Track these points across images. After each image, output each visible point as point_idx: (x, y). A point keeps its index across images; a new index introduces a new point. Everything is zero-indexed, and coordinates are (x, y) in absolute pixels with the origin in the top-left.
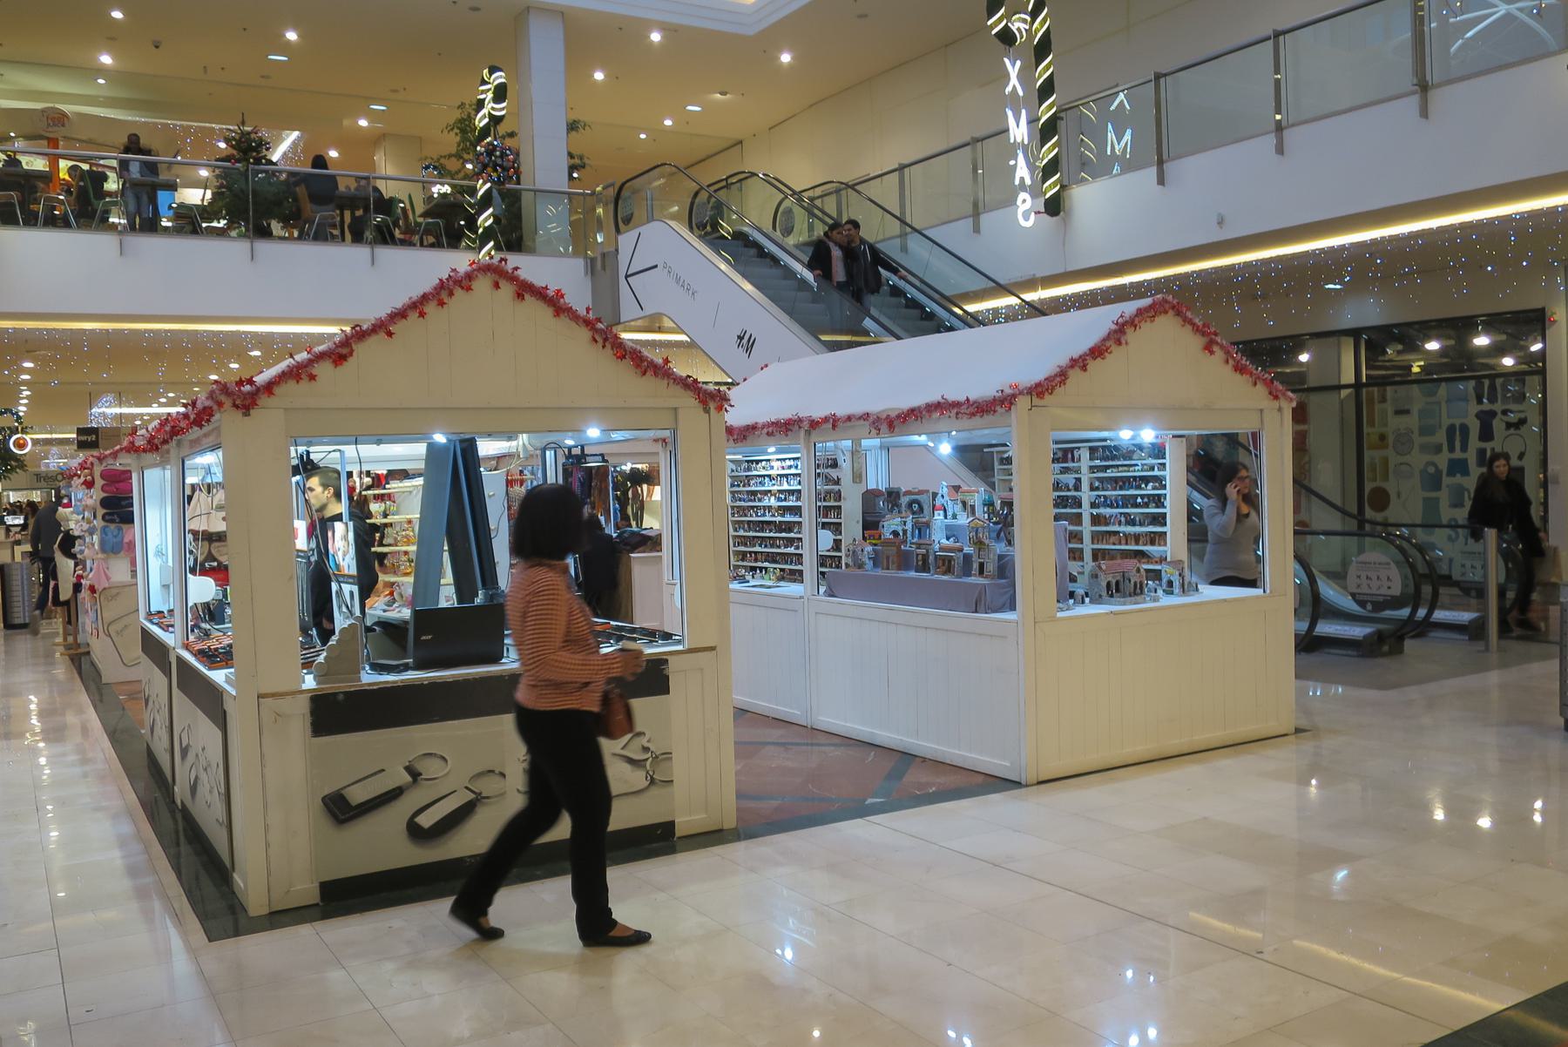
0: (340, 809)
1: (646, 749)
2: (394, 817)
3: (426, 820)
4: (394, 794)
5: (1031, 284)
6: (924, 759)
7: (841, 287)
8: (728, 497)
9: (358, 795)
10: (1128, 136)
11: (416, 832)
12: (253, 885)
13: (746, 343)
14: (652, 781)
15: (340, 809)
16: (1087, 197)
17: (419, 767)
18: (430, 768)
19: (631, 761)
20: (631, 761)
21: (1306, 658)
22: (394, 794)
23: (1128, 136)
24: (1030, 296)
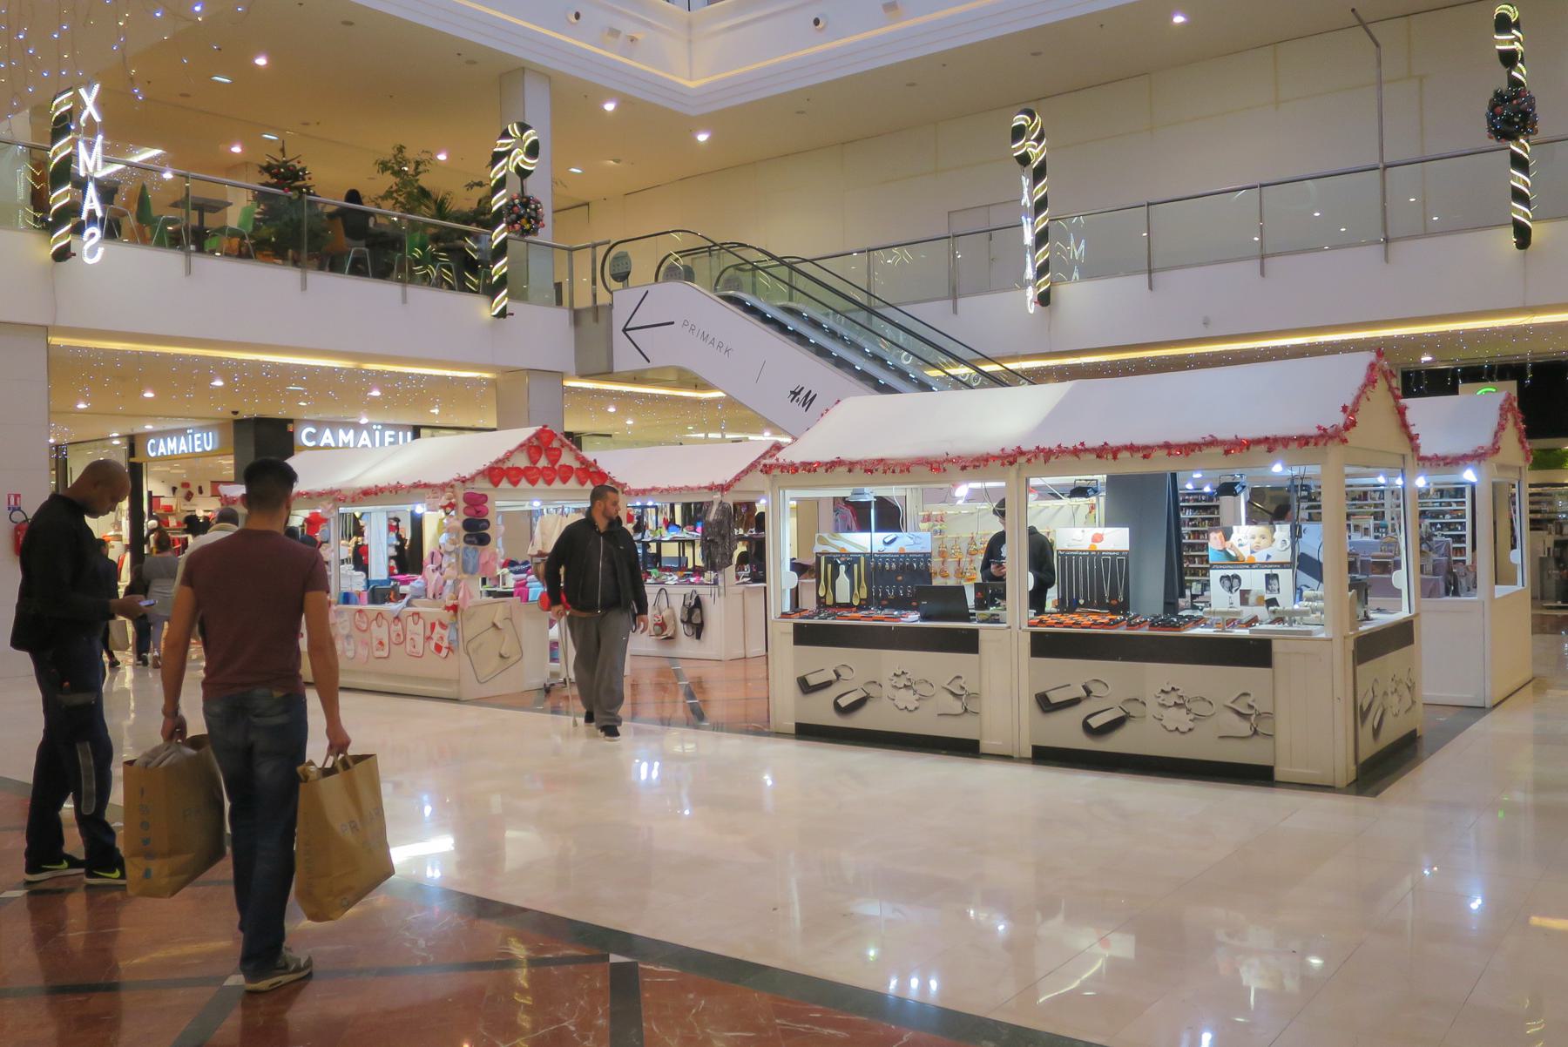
0: (1045, 704)
1: (1251, 707)
2: (1076, 715)
3: (844, 702)
4: (827, 684)
5: (1015, 358)
6: (729, 730)
7: (795, 439)
8: (1366, 539)
9: (1055, 697)
10: (1082, 246)
11: (839, 709)
12: (715, 711)
13: (201, 491)
14: (1256, 732)
15: (1045, 704)
16: (1074, 294)
17: (1092, 687)
18: (844, 673)
19: (1238, 713)
20: (1238, 713)
21: (1537, 636)
22: (827, 684)
23: (1082, 246)
24: (1012, 366)
